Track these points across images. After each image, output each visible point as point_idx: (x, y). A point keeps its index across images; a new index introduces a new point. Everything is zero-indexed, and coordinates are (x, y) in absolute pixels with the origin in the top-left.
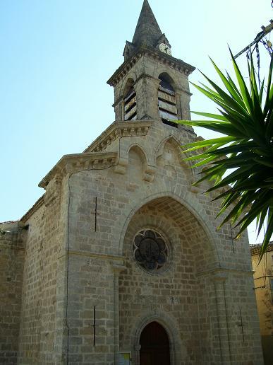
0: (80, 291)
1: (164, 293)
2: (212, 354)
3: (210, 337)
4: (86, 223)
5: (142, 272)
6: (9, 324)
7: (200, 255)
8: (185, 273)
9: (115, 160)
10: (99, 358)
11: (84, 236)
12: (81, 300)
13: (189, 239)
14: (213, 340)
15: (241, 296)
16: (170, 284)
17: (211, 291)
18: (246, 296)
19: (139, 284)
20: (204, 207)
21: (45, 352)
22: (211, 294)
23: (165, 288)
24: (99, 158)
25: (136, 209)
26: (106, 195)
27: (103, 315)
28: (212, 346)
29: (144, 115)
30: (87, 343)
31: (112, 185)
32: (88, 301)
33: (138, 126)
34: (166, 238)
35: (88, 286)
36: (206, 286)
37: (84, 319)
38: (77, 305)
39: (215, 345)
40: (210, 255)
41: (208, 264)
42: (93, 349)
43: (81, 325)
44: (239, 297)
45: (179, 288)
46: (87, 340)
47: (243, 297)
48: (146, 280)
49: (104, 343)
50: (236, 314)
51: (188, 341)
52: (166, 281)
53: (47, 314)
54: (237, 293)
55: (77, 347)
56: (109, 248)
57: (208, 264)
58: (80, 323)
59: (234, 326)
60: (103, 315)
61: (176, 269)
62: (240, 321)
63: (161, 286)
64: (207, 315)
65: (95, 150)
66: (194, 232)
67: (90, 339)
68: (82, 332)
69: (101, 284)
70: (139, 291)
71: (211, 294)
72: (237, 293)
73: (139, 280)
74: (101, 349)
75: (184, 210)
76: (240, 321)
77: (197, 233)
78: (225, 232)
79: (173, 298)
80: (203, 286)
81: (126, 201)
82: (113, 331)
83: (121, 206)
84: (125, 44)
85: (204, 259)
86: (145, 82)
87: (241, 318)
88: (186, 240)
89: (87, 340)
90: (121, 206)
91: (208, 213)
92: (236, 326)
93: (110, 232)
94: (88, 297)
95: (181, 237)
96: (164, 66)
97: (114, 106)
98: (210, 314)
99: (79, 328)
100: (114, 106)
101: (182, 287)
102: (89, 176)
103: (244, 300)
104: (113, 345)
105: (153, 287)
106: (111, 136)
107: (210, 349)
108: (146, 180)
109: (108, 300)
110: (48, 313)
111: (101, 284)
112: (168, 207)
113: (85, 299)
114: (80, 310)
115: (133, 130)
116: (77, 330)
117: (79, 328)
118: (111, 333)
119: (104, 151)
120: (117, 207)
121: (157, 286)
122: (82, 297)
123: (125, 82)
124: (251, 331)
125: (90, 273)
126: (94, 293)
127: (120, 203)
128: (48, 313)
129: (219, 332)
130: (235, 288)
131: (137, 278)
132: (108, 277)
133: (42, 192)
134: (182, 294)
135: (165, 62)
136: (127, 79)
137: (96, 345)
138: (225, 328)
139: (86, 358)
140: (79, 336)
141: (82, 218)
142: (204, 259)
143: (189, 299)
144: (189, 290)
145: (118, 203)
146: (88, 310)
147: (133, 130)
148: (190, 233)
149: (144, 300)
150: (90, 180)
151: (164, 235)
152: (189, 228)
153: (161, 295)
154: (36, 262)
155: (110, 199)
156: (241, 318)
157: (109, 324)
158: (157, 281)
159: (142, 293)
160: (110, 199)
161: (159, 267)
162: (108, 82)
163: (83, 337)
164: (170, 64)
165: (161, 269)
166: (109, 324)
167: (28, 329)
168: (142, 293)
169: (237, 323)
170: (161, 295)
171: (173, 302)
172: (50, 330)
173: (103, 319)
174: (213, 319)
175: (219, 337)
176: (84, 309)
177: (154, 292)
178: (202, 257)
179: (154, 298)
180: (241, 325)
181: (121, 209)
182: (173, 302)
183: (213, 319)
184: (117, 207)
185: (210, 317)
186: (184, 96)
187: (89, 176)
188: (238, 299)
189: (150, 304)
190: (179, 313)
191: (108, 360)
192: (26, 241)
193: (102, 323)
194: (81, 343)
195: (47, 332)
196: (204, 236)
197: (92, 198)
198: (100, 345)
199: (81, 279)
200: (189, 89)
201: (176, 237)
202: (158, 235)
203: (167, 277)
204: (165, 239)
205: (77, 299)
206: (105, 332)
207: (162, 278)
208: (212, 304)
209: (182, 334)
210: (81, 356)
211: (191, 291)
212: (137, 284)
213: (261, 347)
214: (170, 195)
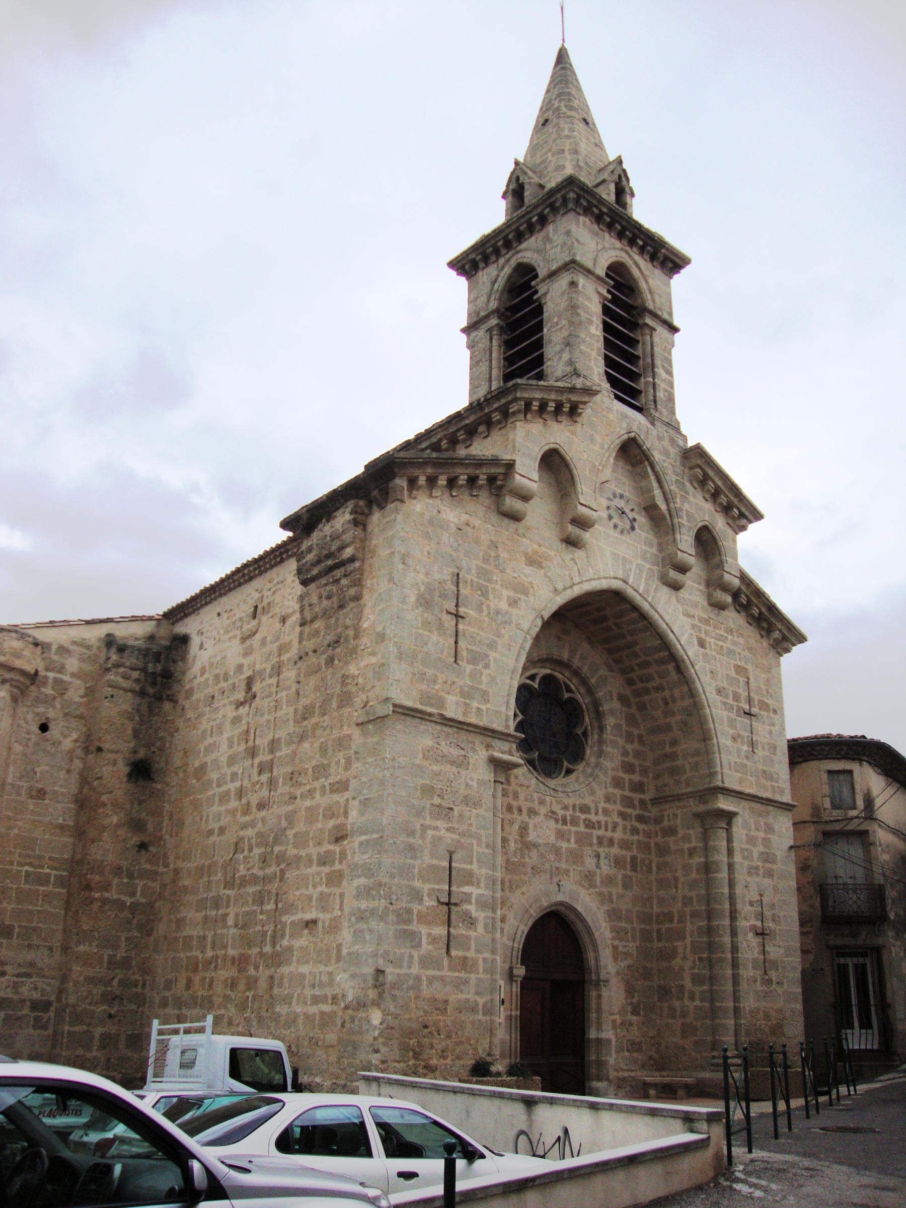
0: (419, 813)
1: (582, 840)
2: (687, 1002)
3: (685, 958)
4: (435, 638)
5: (534, 781)
6: (129, 901)
7: (668, 749)
8: (627, 793)
9: (504, 480)
10: (459, 985)
11: (430, 672)
12: (423, 837)
13: (642, 707)
14: (692, 968)
15: (765, 861)
16: (593, 818)
17: (694, 844)
18: (774, 862)
19: (525, 811)
20: (693, 626)
21: (305, 969)
22: (692, 852)
23: (582, 828)
24: (470, 471)
25: (547, 614)
26: (479, 568)
27: (469, 878)
28: (687, 983)
29: (569, 369)
30: (431, 947)
31: (494, 545)
32: (437, 840)
33: (564, 398)
34: (587, 700)
35: (437, 801)
36: (681, 832)
37: (427, 886)
38: (411, 848)
39: (697, 980)
40: (697, 753)
41: (689, 774)
42: (446, 962)
43: (421, 900)
44: (760, 864)
45: (614, 829)
46: (434, 940)
47: (767, 865)
48: (542, 802)
49: (469, 949)
50: (751, 904)
51: (629, 967)
52: (585, 809)
53: (310, 871)
54: (755, 854)
55: (411, 956)
56: (484, 707)
57: (689, 774)
58: (417, 896)
59: (746, 934)
60: (469, 878)
61: (609, 781)
62: (759, 924)
63: (574, 822)
64: (680, 905)
65: (436, 447)
66: (659, 688)
67: (441, 937)
68: (421, 919)
69: (466, 800)
70: (524, 829)
71: (692, 852)
72: (755, 854)
73: (526, 800)
74: (464, 964)
75: (646, 629)
76: (759, 924)
77: (667, 693)
78: (736, 697)
79: (598, 856)
80: (671, 831)
81: (524, 590)
82: (489, 921)
83: (513, 603)
84: (512, 166)
85: (679, 762)
86: (573, 284)
87: (761, 916)
88: (634, 710)
89: (434, 940)
90: (513, 603)
91: (702, 644)
92: (751, 935)
93: (487, 666)
94: (436, 828)
95: (623, 699)
96: (618, 244)
97: (466, 330)
98: (687, 901)
99: (416, 907)
100: (466, 330)
101: (619, 829)
102: (444, 515)
103: (770, 874)
104: (487, 955)
105: (557, 821)
106: (496, 417)
107: (682, 988)
108: (571, 542)
109: (479, 839)
110: (315, 868)
111: (466, 800)
112: (605, 619)
113: (430, 833)
114: (418, 862)
115: (551, 406)
116: (409, 911)
117: (416, 907)
118: (486, 926)
119: (462, 452)
120: (503, 605)
121: (565, 822)
122: (424, 828)
123: (507, 270)
124: (782, 951)
125: (443, 768)
126: (449, 820)
127: (512, 594)
128: (315, 868)
129: (711, 946)
130: (751, 840)
131: (522, 797)
132: (480, 783)
133: (287, 535)
134: (621, 847)
135: (620, 236)
136: (513, 262)
137: (454, 953)
138: (727, 939)
139: (430, 983)
140: (413, 927)
141: (426, 624)
142: (679, 762)
143: (634, 859)
144: (636, 838)
145: (506, 593)
146: (435, 862)
147: (551, 406)
148: (647, 691)
149: (534, 853)
150: (443, 526)
151: (582, 690)
152: (649, 678)
153: (573, 845)
154: (226, 735)
155: (489, 580)
156: (761, 916)
157: (482, 904)
158: (565, 808)
159: (532, 836)
160: (489, 580)
161: (569, 772)
162: (452, 264)
163: (424, 930)
164: (632, 242)
165: (573, 776)
166: (482, 904)
167: (192, 915)
168: (532, 836)
169: (753, 928)
170: (573, 845)
171: (598, 866)
172: (324, 909)
173: (467, 889)
174: (695, 915)
175: (710, 960)
176: (427, 860)
177: (560, 835)
178: (673, 756)
179: (557, 851)
180: (761, 933)
181: (514, 611)
182: (598, 866)
183: (695, 915)
184: (503, 605)
185: (688, 910)
186: (661, 331)
187: (444, 515)
188: (757, 868)
189: (547, 866)
190: (610, 893)
191: (477, 993)
192: (184, 673)
193: (467, 898)
194: (419, 945)
195: (309, 916)
196: (686, 703)
197: (444, 574)
198: (461, 953)
199: (421, 781)
200: (671, 314)
201: (611, 699)
202: (569, 690)
203: (588, 800)
204: (584, 700)
205: (412, 833)
206: (471, 922)
207: (578, 801)
208: (694, 875)
209: (615, 948)
210: (418, 978)
211: (639, 842)
212: (520, 810)
213: (799, 990)
214: (616, 584)
